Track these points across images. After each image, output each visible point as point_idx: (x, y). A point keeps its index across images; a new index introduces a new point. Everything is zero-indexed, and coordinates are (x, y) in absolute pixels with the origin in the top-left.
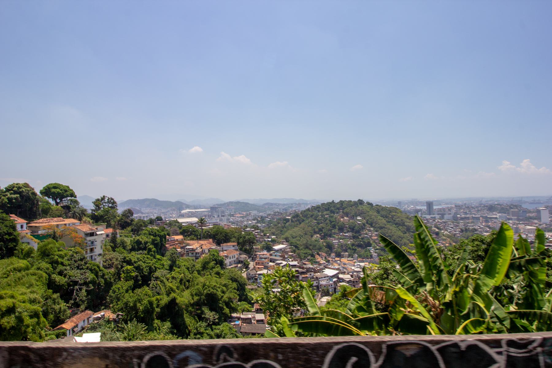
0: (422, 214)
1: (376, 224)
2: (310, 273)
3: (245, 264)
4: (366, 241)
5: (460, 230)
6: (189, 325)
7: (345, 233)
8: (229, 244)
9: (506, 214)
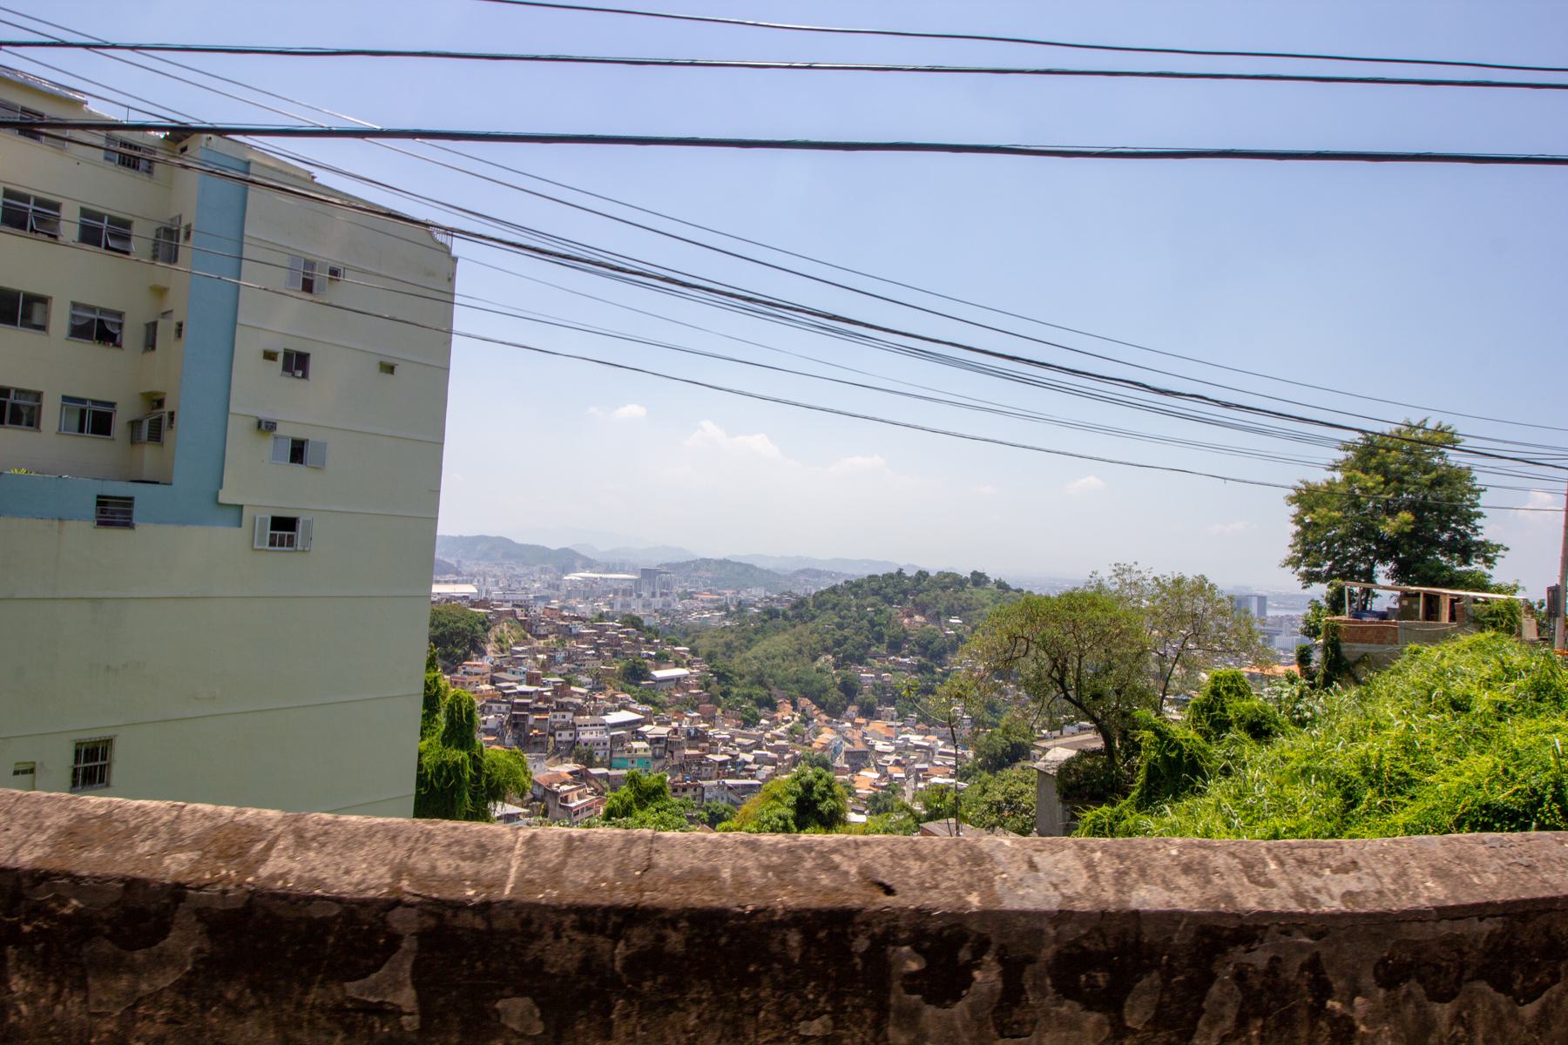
7: (903, 657)
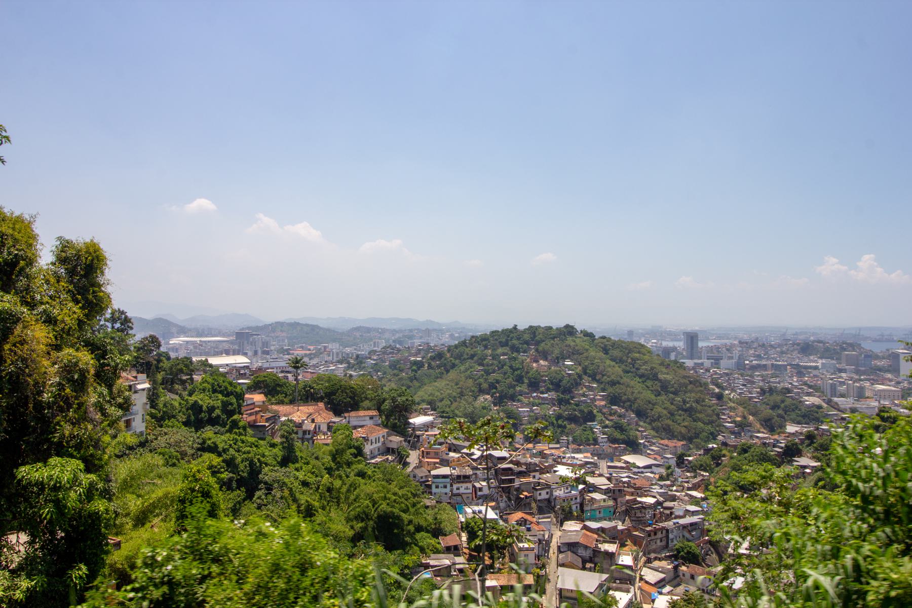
1: (603, 375)
2: (534, 474)
4: (586, 410)
5: (758, 390)
7: (542, 393)
8: (361, 413)
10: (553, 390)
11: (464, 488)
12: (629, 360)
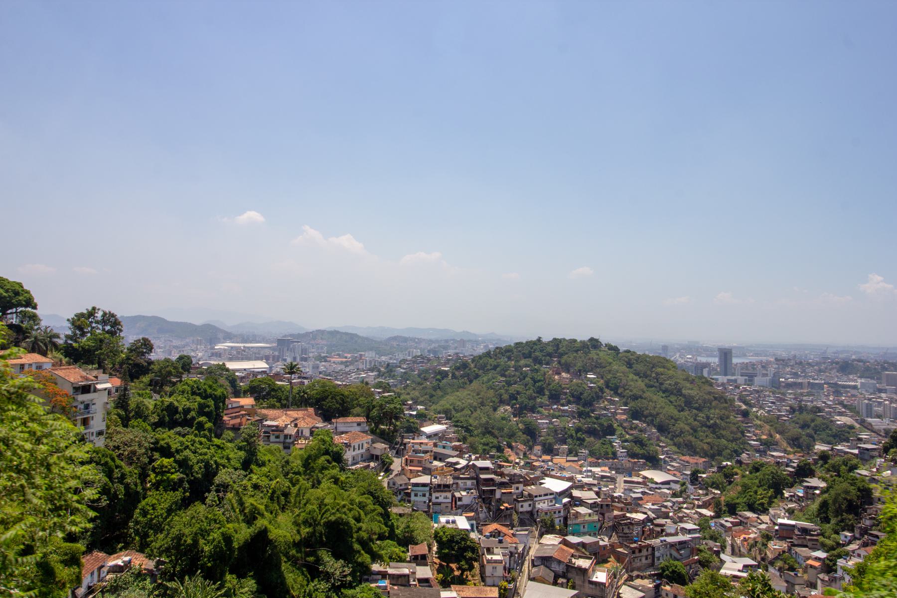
0: (709, 373)
1: (625, 390)
2: (517, 485)
3: (383, 462)
4: (606, 424)
5: (788, 408)
6: (293, 588)
7: (563, 405)
8: (350, 419)
9: (874, 379)
10: (573, 402)
11: (443, 497)
12: (654, 375)
